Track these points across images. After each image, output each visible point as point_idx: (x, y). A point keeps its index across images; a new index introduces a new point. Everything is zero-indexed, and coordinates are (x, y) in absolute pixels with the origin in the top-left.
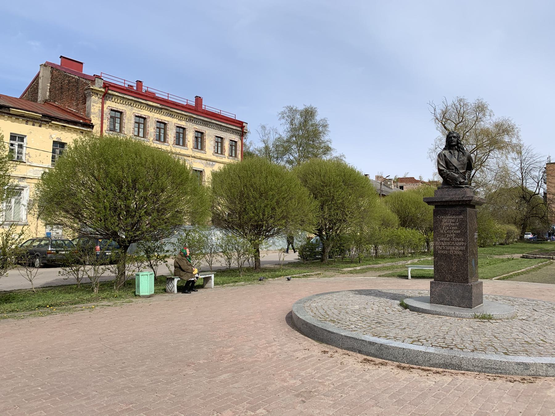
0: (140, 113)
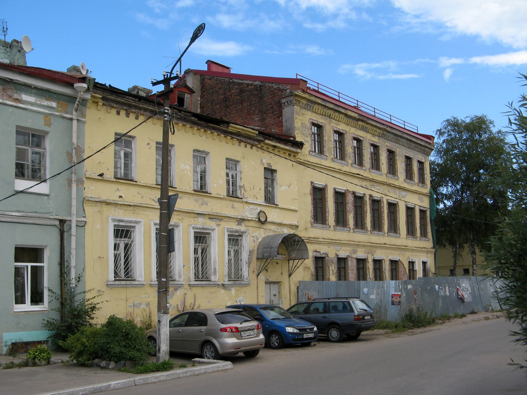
0: (338, 127)
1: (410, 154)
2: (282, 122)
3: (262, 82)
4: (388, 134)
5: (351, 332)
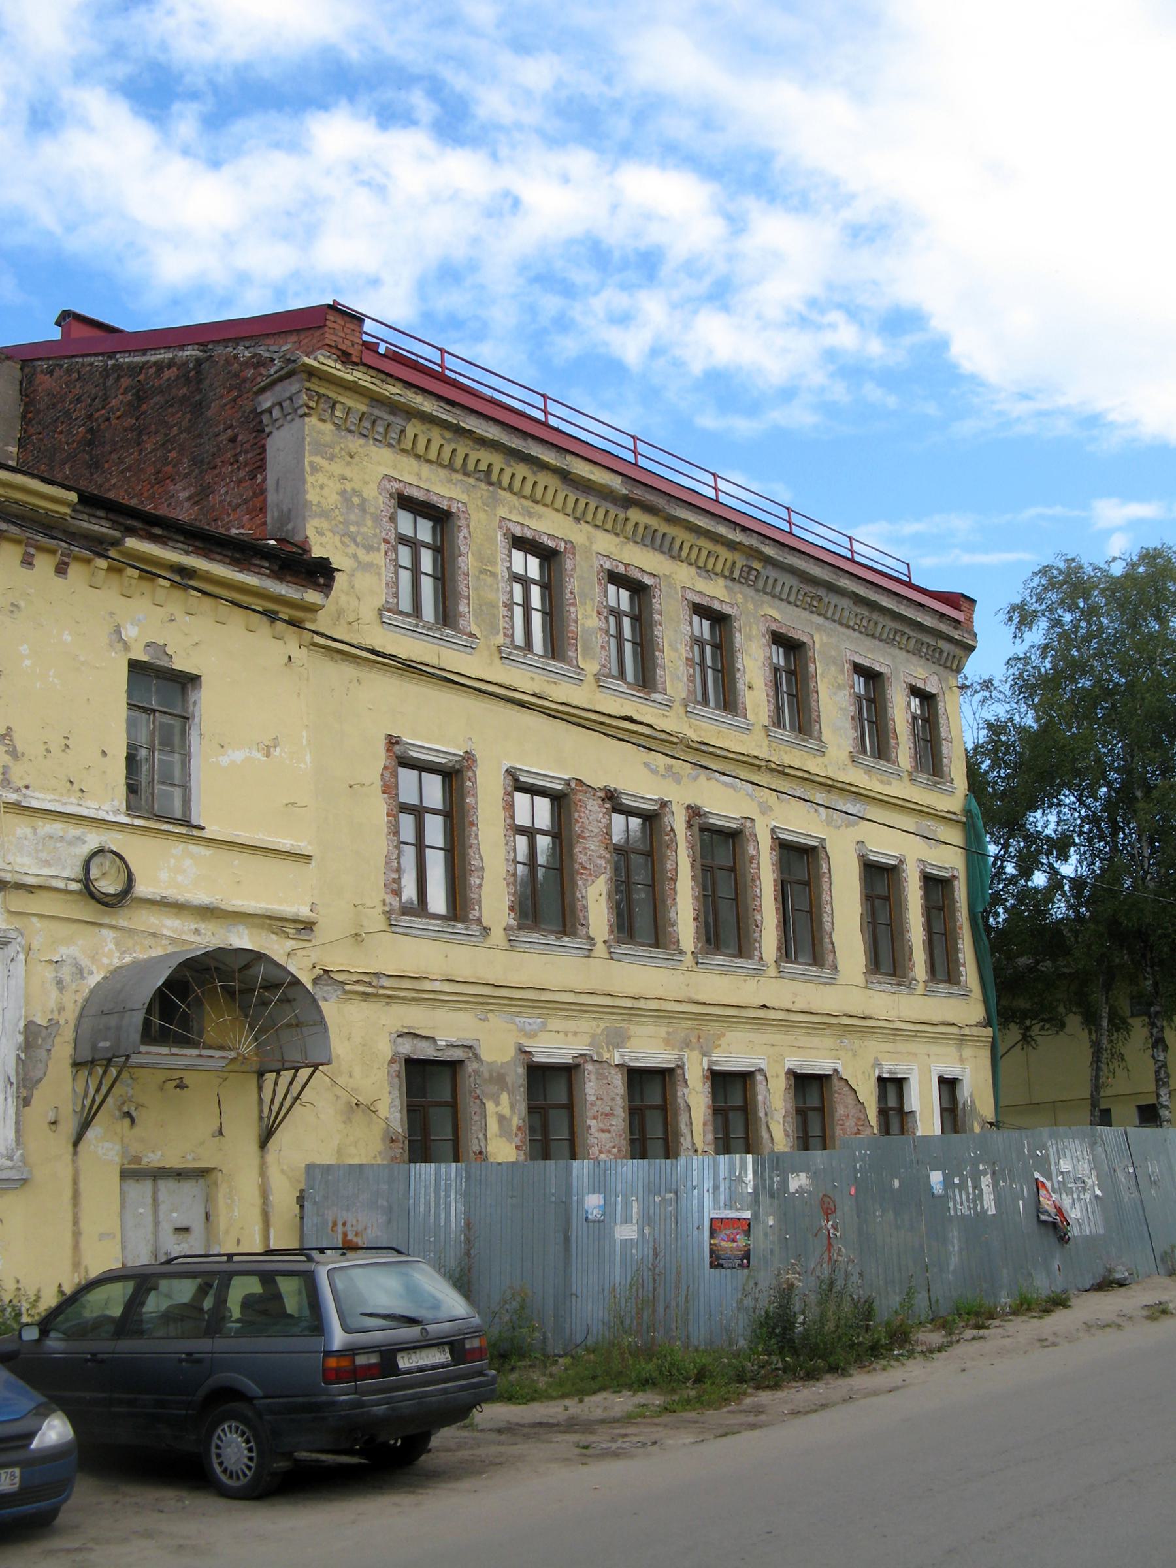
0: (533, 524)
1: (878, 658)
2: (263, 492)
3: (203, 346)
4: (773, 573)
5: (362, 1437)
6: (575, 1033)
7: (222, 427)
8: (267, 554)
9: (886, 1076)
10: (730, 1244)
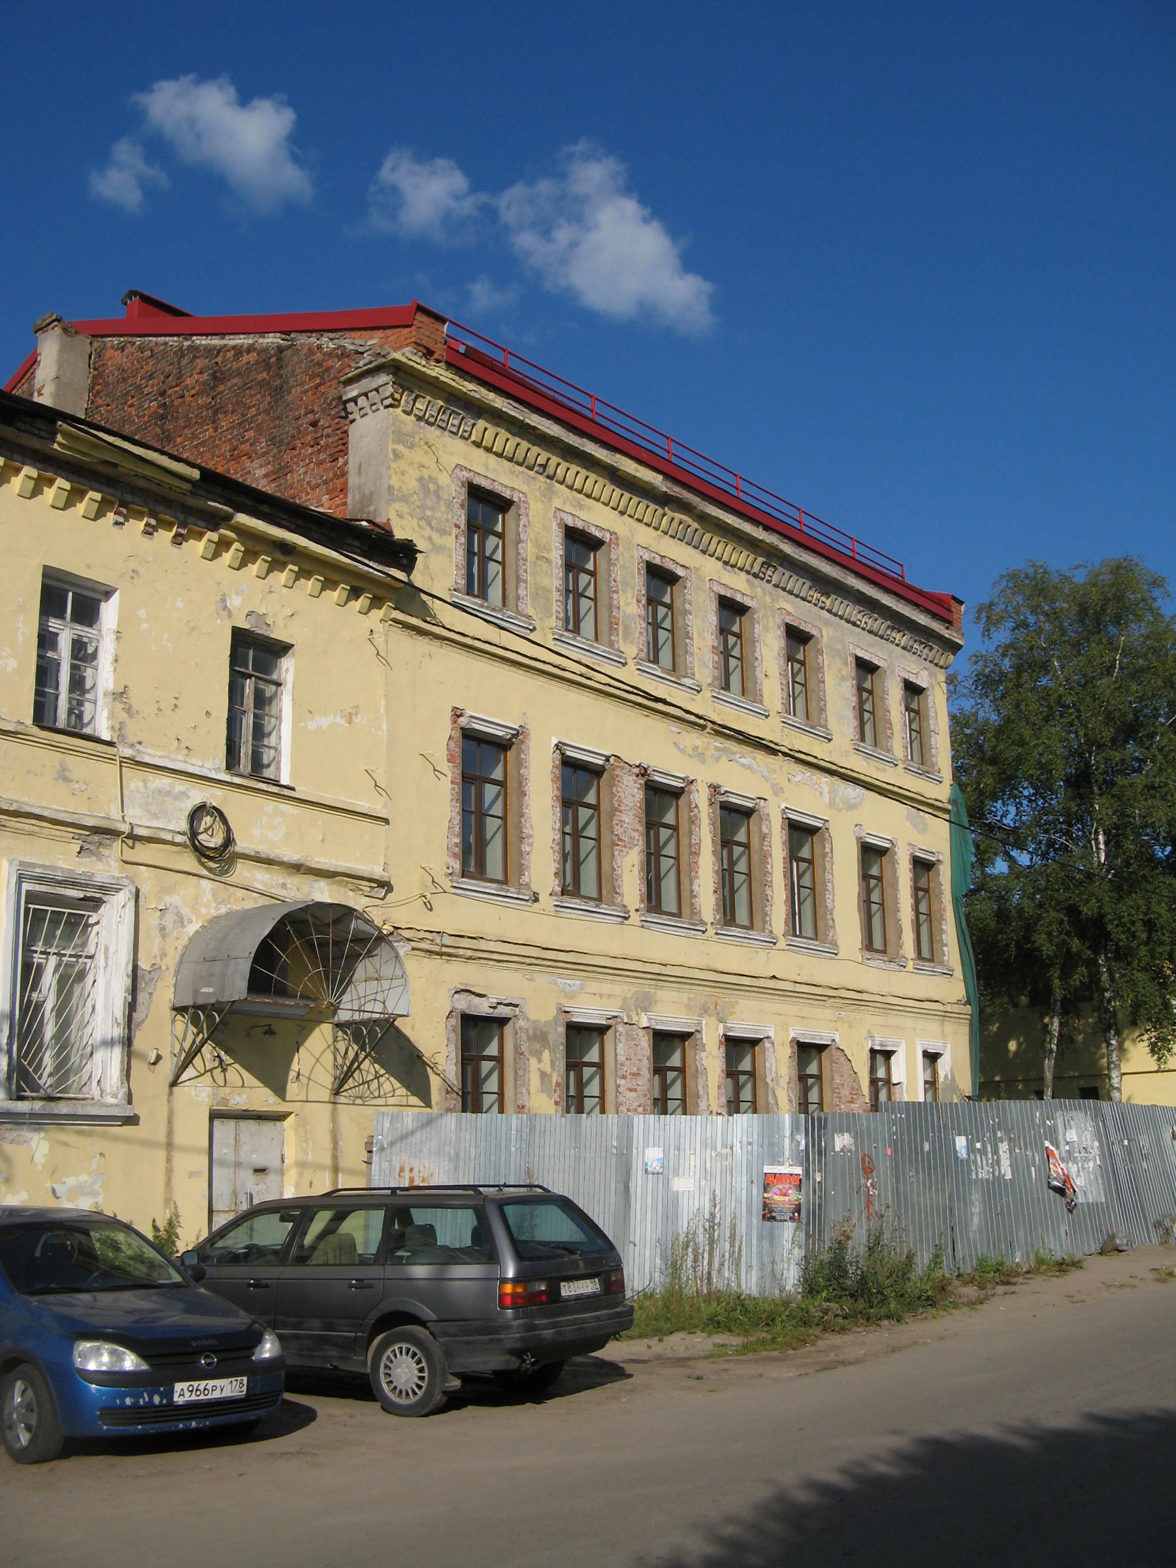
0: (583, 515)
1: (875, 652)
2: (344, 474)
6: (609, 996)
7: (303, 412)
8: (360, 534)
9: (877, 1048)
10: (781, 1198)
